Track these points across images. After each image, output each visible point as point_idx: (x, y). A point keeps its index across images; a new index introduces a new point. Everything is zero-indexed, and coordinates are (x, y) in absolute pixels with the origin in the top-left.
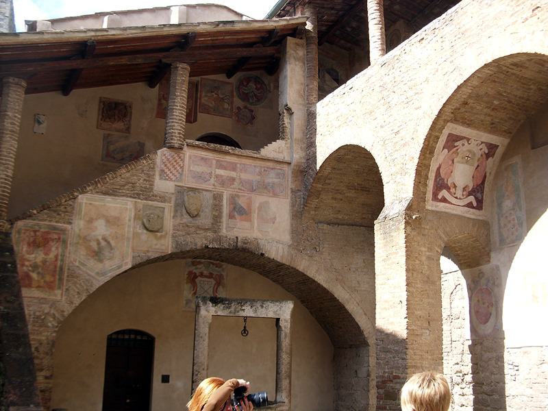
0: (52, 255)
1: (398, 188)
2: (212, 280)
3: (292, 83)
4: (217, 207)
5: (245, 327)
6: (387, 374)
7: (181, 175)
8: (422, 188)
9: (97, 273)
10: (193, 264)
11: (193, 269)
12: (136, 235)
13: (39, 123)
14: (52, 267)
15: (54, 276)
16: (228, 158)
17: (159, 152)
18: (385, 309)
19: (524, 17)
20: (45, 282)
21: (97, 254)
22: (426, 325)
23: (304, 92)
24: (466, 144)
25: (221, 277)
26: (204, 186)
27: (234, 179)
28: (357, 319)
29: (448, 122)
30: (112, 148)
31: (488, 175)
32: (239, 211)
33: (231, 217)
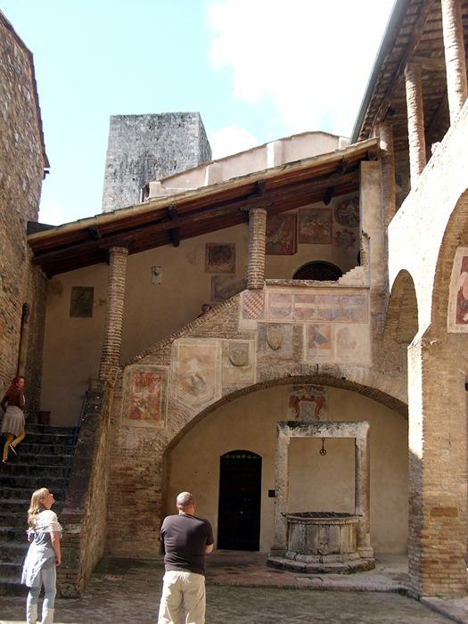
0: (155, 393)
2: (314, 402)
3: (367, 208)
8: (441, 314)
10: (295, 389)
11: (295, 393)
12: (224, 370)
13: (156, 274)
14: (156, 402)
15: (158, 409)
16: (307, 291)
17: (241, 294)
20: (151, 414)
21: (192, 389)
22: (445, 445)
23: (381, 214)
25: (322, 399)
27: (313, 311)
29: (457, 247)
30: (219, 288)
32: (319, 340)
33: (311, 346)
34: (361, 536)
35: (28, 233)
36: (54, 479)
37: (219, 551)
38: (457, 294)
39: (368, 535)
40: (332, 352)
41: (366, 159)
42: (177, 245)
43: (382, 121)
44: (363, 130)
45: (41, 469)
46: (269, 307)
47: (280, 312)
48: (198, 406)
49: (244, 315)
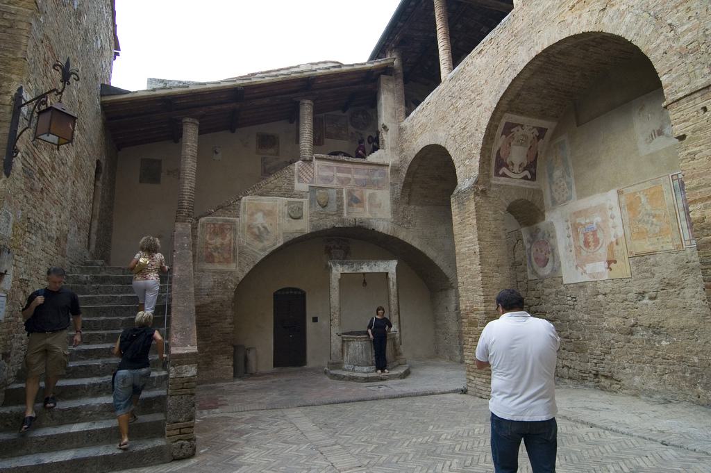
1: (467, 171)
4: (340, 199)
5: (364, 280)
6: (468, 308)
7: (313, 179)
9: (260, 250)
13: (216, 153)
16: (344, 165)
18: (463, 259)
19: (571, 4)
20: (224, 258)
21: (258, 237)
24: (520, 129)
26: (329, 185)
27: (350, 179)
28: (445, 271)
30: (267, 166)
31: (539, 153)
32: (355, 201)
33: (349, 205)
34: (397, 348)
35: (102, 95)
37: (275, 368)
38: (496, 153)
40: (365, 210)
41: (385, 73)
42: (233, 131)
43: (395, 48)
44: (379, 52)
46: (318, 175)
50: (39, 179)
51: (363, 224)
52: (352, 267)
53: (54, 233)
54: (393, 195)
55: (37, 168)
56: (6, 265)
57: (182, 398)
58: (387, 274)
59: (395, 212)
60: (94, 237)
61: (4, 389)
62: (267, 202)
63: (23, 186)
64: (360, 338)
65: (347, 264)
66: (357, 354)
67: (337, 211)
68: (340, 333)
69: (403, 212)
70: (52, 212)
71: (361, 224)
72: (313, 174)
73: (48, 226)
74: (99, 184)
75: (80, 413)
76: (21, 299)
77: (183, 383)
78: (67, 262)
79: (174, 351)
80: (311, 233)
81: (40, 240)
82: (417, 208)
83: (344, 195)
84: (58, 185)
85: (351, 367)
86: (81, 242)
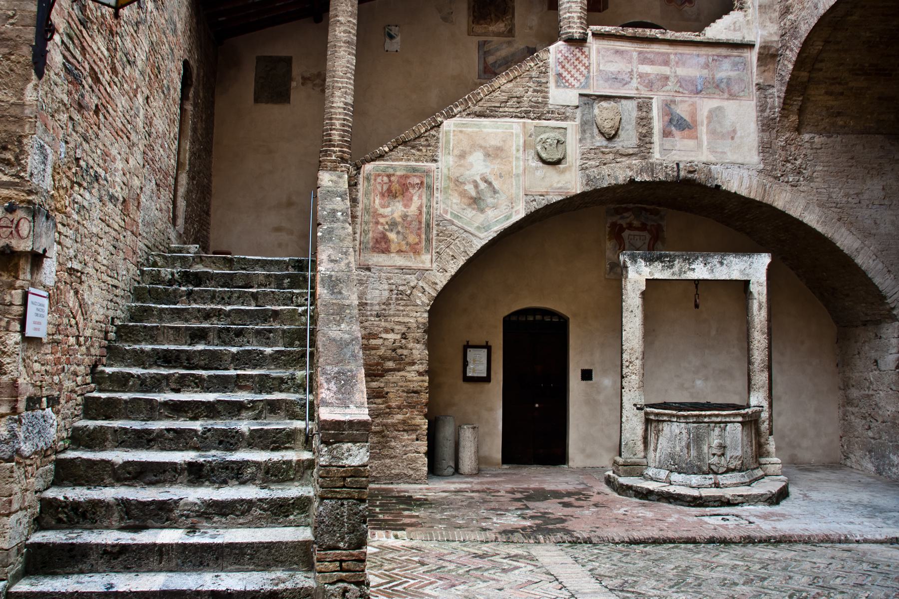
2: (645, 233)
4: (644, 121)
7: (587, 78)
9: (478, 228)
10: (617, 212)
13: (391, 37)
20: (407, 244)
21: (476, 202)
27: (667, 78)
30: (491, 59)
33: (666, 134)
34: (763, 440)
36: (268, 350)
39: (771, 438)
40: (700, 146)
45: (239, 333)
47: (615, 79)
48: (486, 228)
49: (557, 82)
50: (91, 87)
51: (696, 176)
52: (671, 267)
53: (119, 189)
54: (763, 111)
55: (87, 66)
56: (44, 240)
57: (342, 505)
58: (747, 283)
59: (765, 148)
60: (182, 204)
61: (53, 457)
62: (492, 129)
63: (65, 98)
64: (685, 417)
65: (660, 259)
66: (678, 449)
67: (639, 146)
68: (642, 402)
69: (783, 148)
70: (114, 152)
71: (690, 176)
72: (587, 68)
73: (108, 175)
74: (189, 107)
75: (171, 511)
76: (71, 305)
77: (344, 478)
78: (141, 245)
79: (325, 414)
80: (583, 194)
81: (97, 201)
82: (817, 139)
83: (655, 113)
84: (122, 102)
85: (663, 474)
86: (161, 210)
